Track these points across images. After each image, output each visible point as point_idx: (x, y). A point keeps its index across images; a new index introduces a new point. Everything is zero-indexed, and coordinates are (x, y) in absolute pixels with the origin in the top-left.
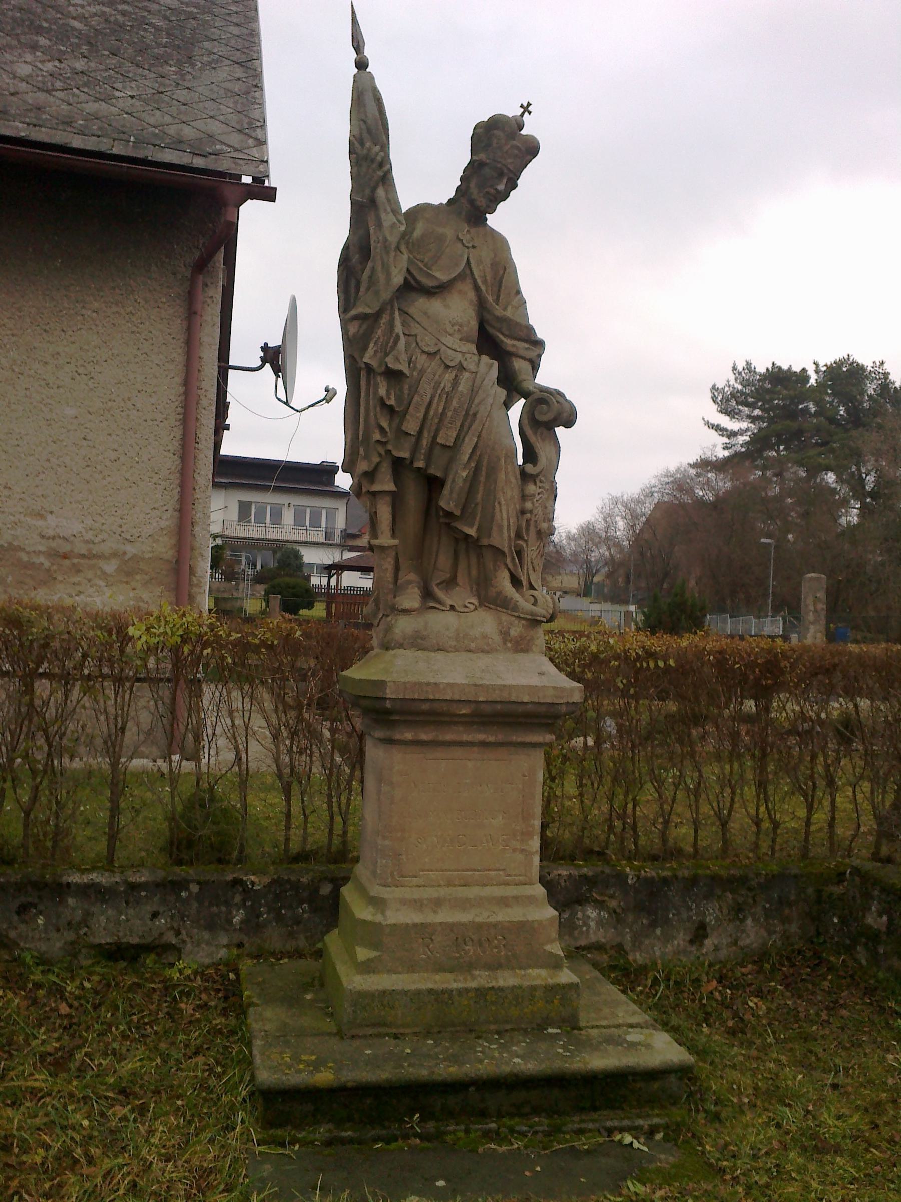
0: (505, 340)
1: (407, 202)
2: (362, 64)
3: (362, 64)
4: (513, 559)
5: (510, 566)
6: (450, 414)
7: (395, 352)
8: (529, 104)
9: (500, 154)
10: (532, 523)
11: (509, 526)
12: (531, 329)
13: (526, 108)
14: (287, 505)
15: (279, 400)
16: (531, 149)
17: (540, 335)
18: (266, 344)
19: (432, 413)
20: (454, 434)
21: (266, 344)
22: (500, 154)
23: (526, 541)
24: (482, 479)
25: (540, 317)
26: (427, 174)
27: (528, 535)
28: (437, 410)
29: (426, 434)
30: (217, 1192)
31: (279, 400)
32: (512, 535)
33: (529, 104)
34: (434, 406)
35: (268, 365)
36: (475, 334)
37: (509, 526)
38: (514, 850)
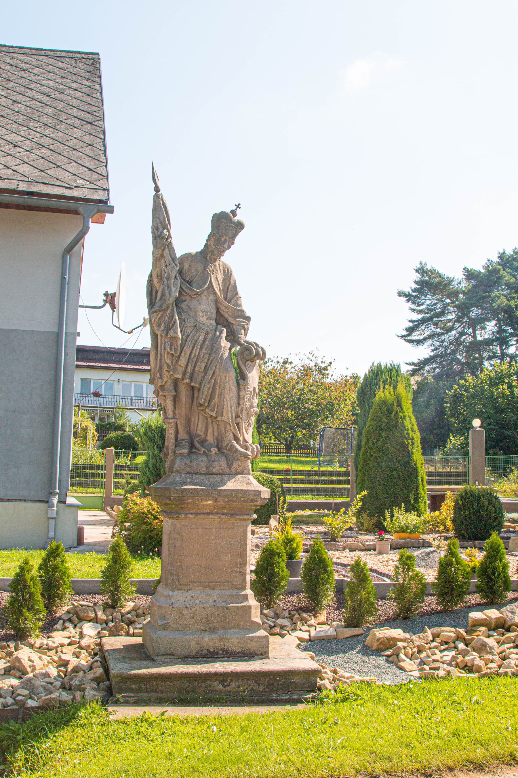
0: (230, 319)
1: (179, 254)
2: (157, 189)
3: (157, 189)
4: (234, 427)
5: (233, 430)
6: (202, 356)
7: (174, 328)
8: (239, 204)
9: (225, 228)
10: (244, 409)
11: (231, 411)
12: (243, 311)
13: (238, 206)
14: (117, 380)
15: (115, 326)
16: (240, 226)
17: (248, 314)
18: (107, 292)
19: (192, 356)
20: (204, 365)
21: (107, 292)
22: (225, 228)
23: (241, 418)
24: (218, 388)
25: (247, 305)
26: (189, 238)
27: (242, 414)
28: (197, 349)
29: (190, 365)
30: (320, 663)
31: (115, 326)
32: (234, 415)
33: (239, 204)
34: (194, 352)
35: (108, 305)
36: (214, 316)
37: (231, 411)
38: (236, 572)
